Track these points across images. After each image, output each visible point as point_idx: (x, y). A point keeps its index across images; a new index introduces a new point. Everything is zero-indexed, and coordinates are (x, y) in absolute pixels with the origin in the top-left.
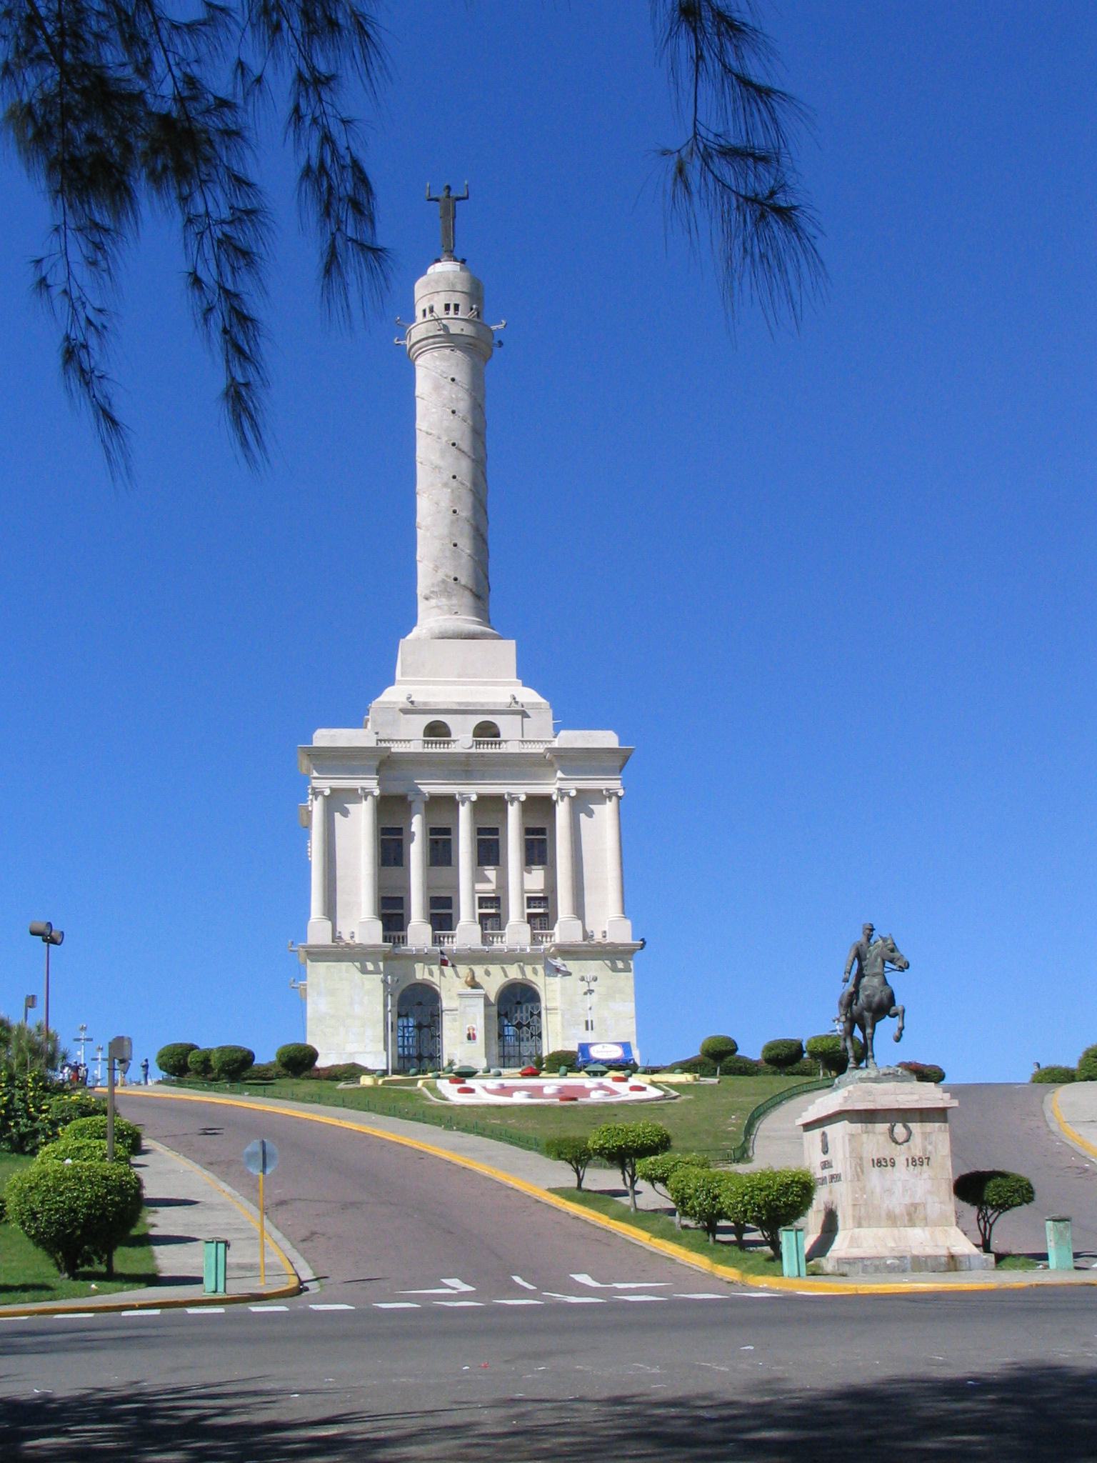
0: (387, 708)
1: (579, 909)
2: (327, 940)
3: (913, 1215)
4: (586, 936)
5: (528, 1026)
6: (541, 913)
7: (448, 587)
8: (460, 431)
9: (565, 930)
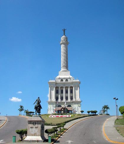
0: (57, 78)
1: (75, 98)
2: (75, 101)
3: (35, 135)
4: (76, 100)
5: (106, 111)
6: (72, 98)
7: (64, 66)
8: (64, 51)
9: (74, 100)
